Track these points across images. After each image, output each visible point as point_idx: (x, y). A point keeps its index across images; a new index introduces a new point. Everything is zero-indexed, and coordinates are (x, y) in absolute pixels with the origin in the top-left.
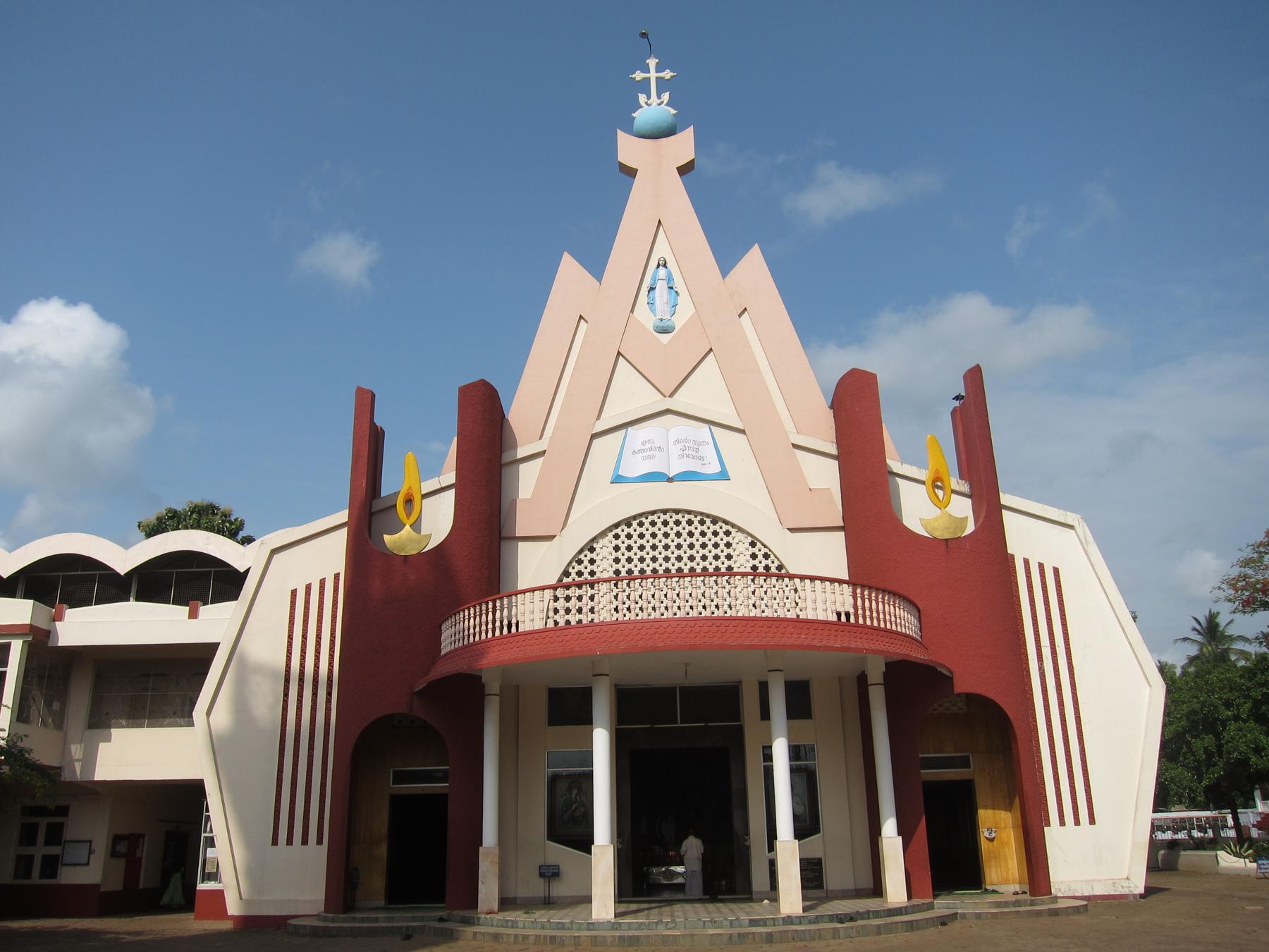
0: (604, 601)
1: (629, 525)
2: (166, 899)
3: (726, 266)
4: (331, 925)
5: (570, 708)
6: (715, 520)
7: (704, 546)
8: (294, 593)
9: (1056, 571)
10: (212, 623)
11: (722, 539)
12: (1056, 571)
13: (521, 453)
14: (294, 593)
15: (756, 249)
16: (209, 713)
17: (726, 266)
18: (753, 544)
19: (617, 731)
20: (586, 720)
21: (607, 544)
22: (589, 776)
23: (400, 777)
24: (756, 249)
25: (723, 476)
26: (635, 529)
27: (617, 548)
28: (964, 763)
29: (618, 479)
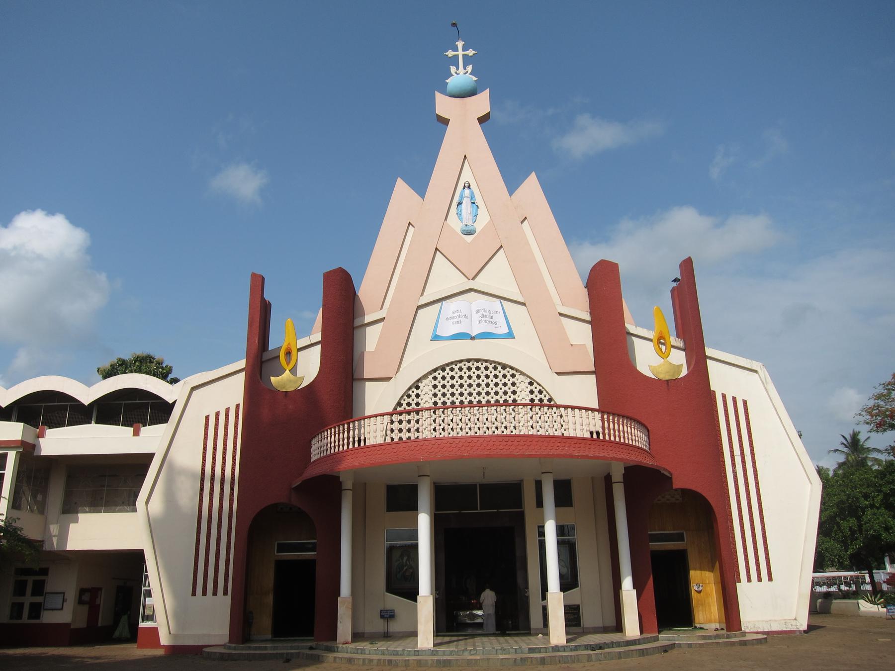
1: (444, 370)
3: (512, 187)
5: (402, 499)
6: (504, 367)
7: (496, 385)
8: (207, 418)
9: (745, 402)
10: (150, 439)
11: (509, 380)
12: (745, 402)
14: (207, 418)
15: (533, 176)
16: (147, 502)
17: (512, 187)
18: (531, 384)
19: (435, 515)
20: (413, 507)
21: (428, 383)
23: (282, 548)
24: (533, 176)
25: (510, 335)
26: (448, 373)
27: (435, 387)
28: (680, 537)
29: (436, 338)
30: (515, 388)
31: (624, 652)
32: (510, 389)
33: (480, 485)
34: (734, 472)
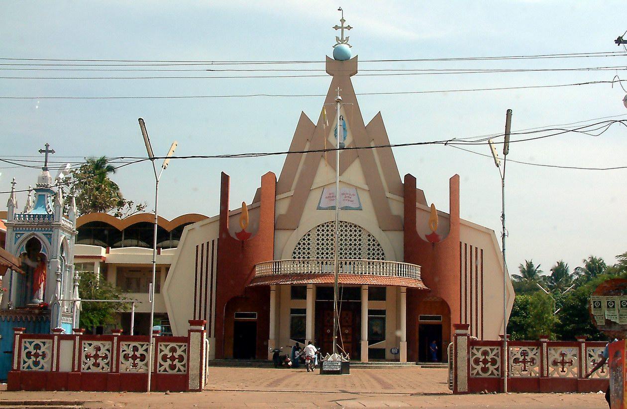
0: (365, 241)
1: (323, 226)
2: (380, 332)
3: (378, 117)
4: (448, 353)
5: (299, 292)
6: (355, 226)
7: (351, 235)
8: (197, 246)
9: (482, 250)
10: (167, 255)
11: (358, 233)
12: (482, 250)
13: (313, 187)
14: (197, 246)
15: (366, 123)
16: (168, 290)
17: (378, 117)
18: (369, 236)
19: (316, 303)
20: (305, 298)
21: (315, 232)
22: (305, 318)
23: (239, 315)
24: (366, 123)
25: (360, 209)
26: (325, 228)
27: (318, 235)
28: (439, 318)
29: (319, 208)
30: (333, 233)
31: (371, 342)
32: (357, 238)
33: (361, 302)
34: (477, 288)
